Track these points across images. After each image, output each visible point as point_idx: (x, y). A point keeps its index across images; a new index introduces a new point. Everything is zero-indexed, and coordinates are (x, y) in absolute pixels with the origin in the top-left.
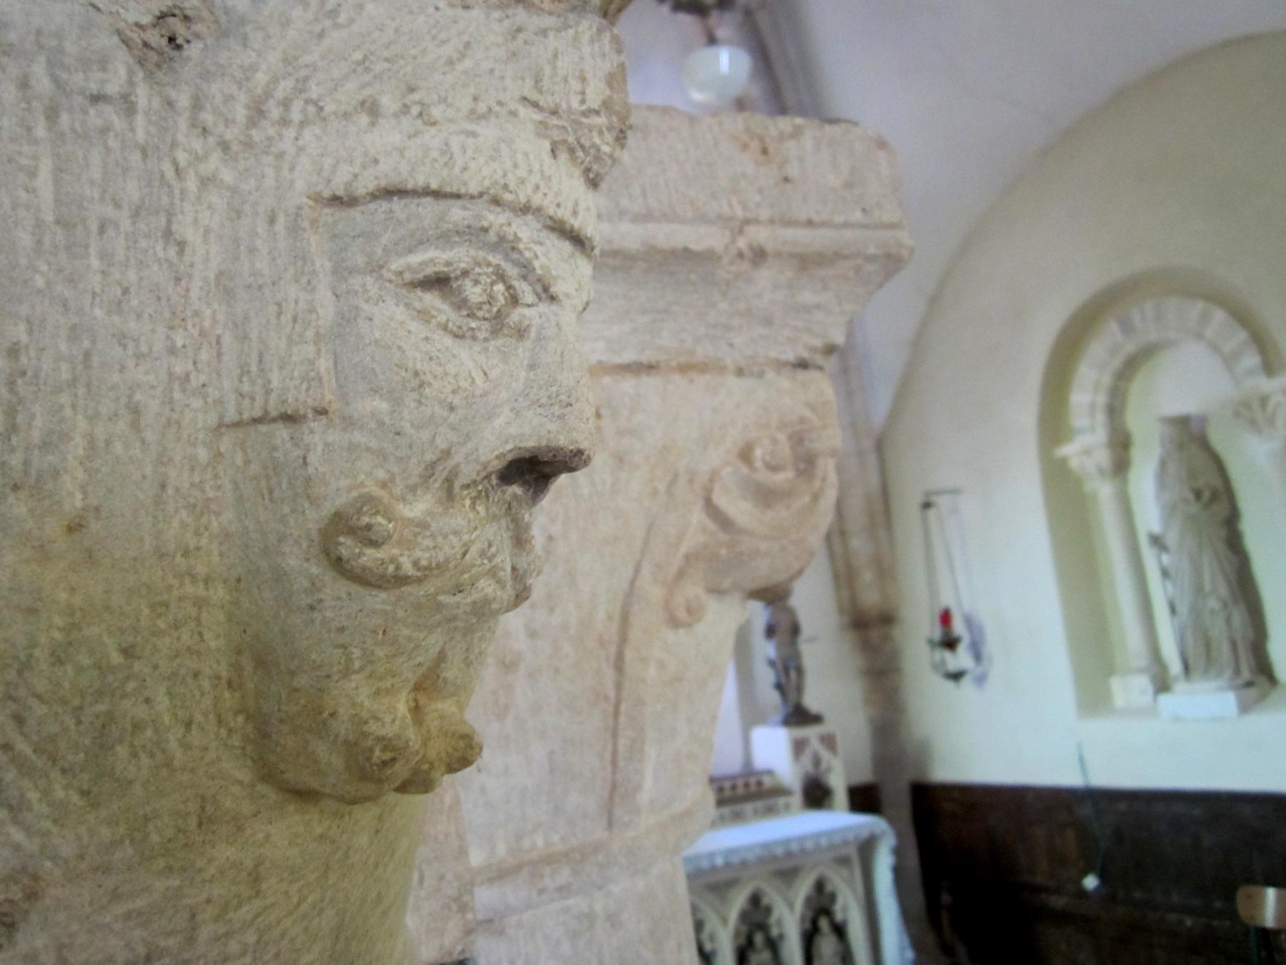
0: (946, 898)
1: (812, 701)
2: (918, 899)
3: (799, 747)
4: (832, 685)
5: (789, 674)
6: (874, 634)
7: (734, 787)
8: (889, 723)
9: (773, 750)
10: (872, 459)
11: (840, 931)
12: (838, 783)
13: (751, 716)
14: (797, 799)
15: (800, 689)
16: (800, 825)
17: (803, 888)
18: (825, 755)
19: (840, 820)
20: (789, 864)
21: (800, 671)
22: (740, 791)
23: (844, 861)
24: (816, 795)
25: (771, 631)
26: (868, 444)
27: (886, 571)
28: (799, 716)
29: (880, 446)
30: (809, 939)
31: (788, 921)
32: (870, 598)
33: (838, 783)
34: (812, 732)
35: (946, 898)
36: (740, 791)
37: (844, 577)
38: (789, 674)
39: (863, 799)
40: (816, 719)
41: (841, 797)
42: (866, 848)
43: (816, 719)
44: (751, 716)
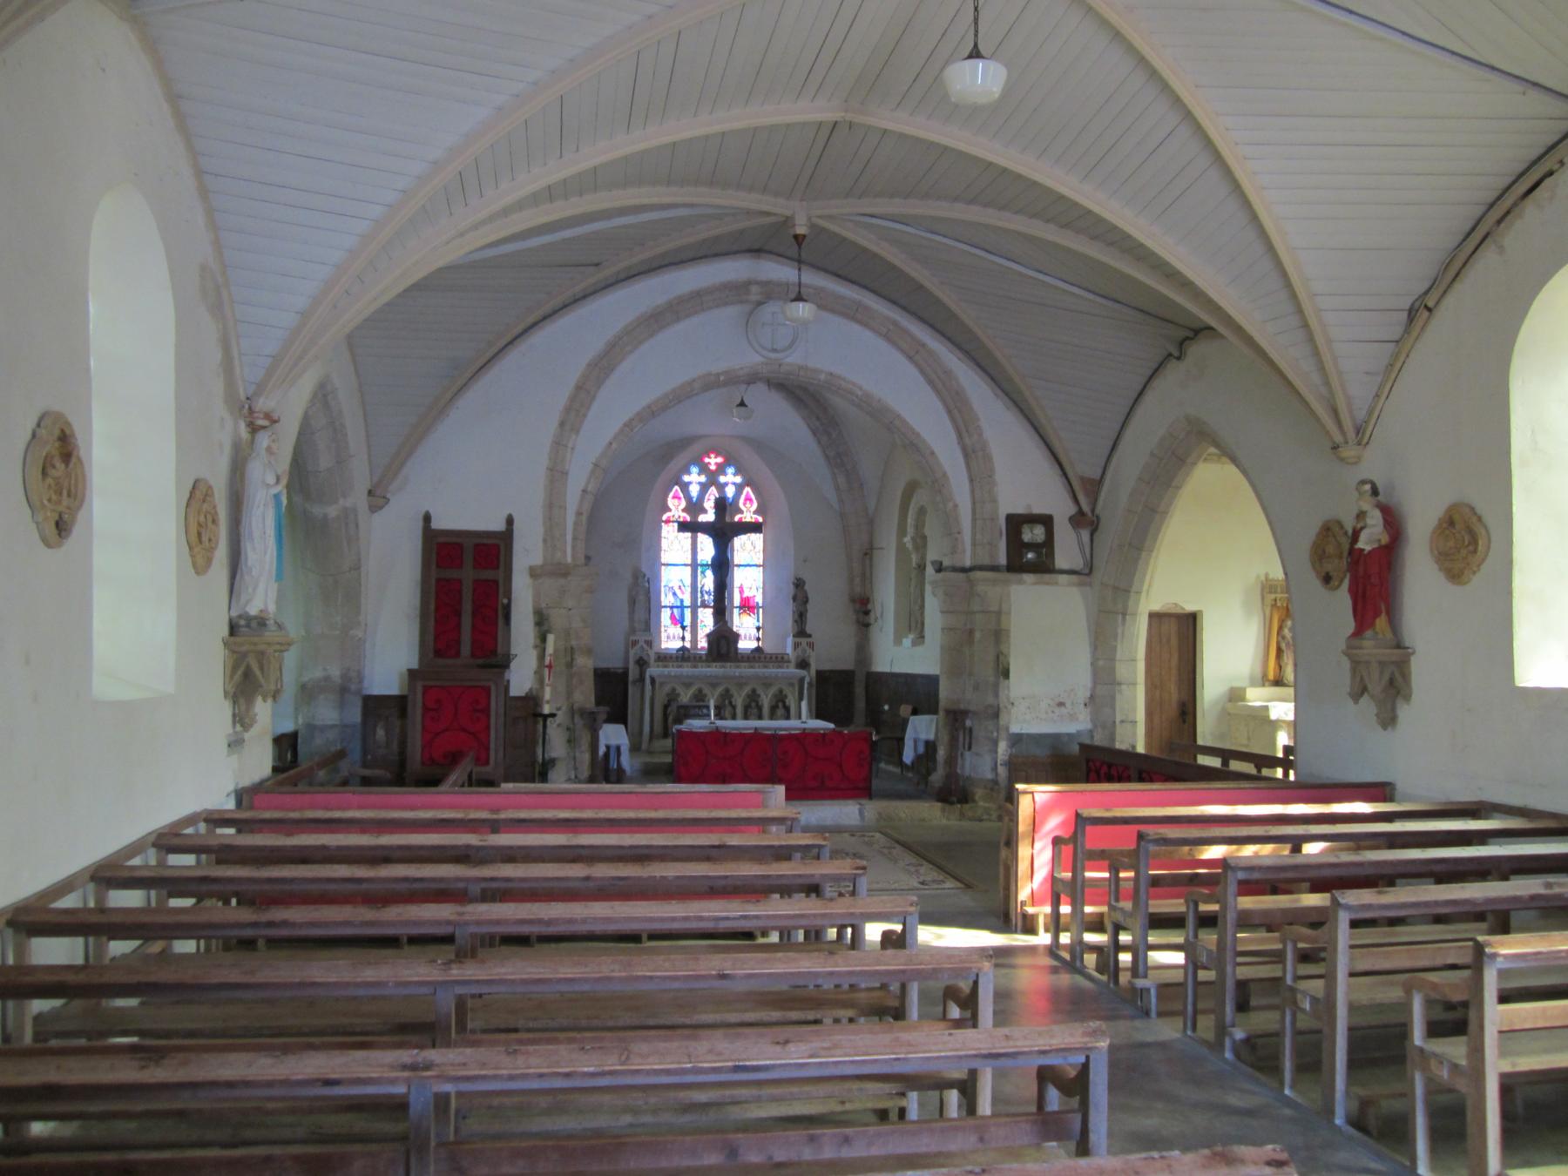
1: (808, 630)
18: (809, 650)
23: (792, 685)
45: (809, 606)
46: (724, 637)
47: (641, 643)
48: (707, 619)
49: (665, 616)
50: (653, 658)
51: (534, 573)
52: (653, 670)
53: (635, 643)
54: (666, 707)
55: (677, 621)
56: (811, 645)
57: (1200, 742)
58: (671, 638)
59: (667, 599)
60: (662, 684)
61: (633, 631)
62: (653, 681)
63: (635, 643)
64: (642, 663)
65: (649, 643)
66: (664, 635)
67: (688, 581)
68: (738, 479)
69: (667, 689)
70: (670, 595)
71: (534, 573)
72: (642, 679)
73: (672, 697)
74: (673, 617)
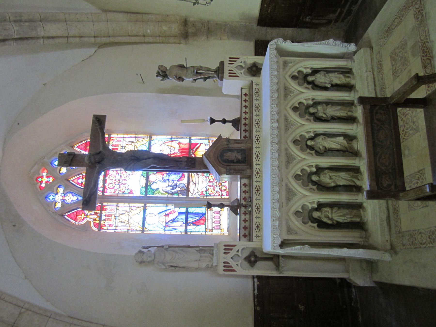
0: (308, 19)
1: (214, 66)
2: (305, 31)
3: (233, 75)
4: (206, 53)
5: (200, 73)
6: (191, 30)
7: (245, 185)
8: (233, 31)
9: (232, 86)
10: (110, 15)
11: (315, 72)
12: (252, 59)
13: (217, 92)
14: (255, 79)
15: (209, 70)
16: (266, 79)
17: (294, 85)
18: (238, 63)
19: (267, 61)
20: (282, 91)
21: (201, 68)
22: (247, 189)
23: (285, 64)
24: (255, 70)
25: (180, 79)
26: (103, 16)
27: (163, 19)
28: (219, 72)
29: (105, 11)
30: (316, 86)
31: (308, 95)
32: (175, 28)
33: (252, 59)
34: (227, 67)
35: (308, 19)
36: (247, 110)
37: (164, 39)
38: (200, 73)
39: (261, 48)
40: (222, 63)
41: (258, 59)
42: (282, 53)
43: (222, 63)
44: (217, 92)
45: (195, 66)
46: (222, 154)
47: (228, 258)
48: (201, 184)
49: (196, 230)
50: (245, 243)
51: (417, 130)
52: (269, 244)
53: (228, 268)
54: (322, 225)
55: (201, 219)
56: (233, 60)
57: (148, 205)
58: (221, 224)
59: (178, 228)
60: (289, 231)
61: (211, 268)
62: (283, 244)
63: (228, 268)
64: (253, 258)
65: (228, 248)
66: (216, 232)
67: (161, 207)
68: (83, 215)
69: (296, 223)
70: (176, 225)
71: (417, 130)
72: (274, 258)
73: (314, 218)
74: (196, 223)
